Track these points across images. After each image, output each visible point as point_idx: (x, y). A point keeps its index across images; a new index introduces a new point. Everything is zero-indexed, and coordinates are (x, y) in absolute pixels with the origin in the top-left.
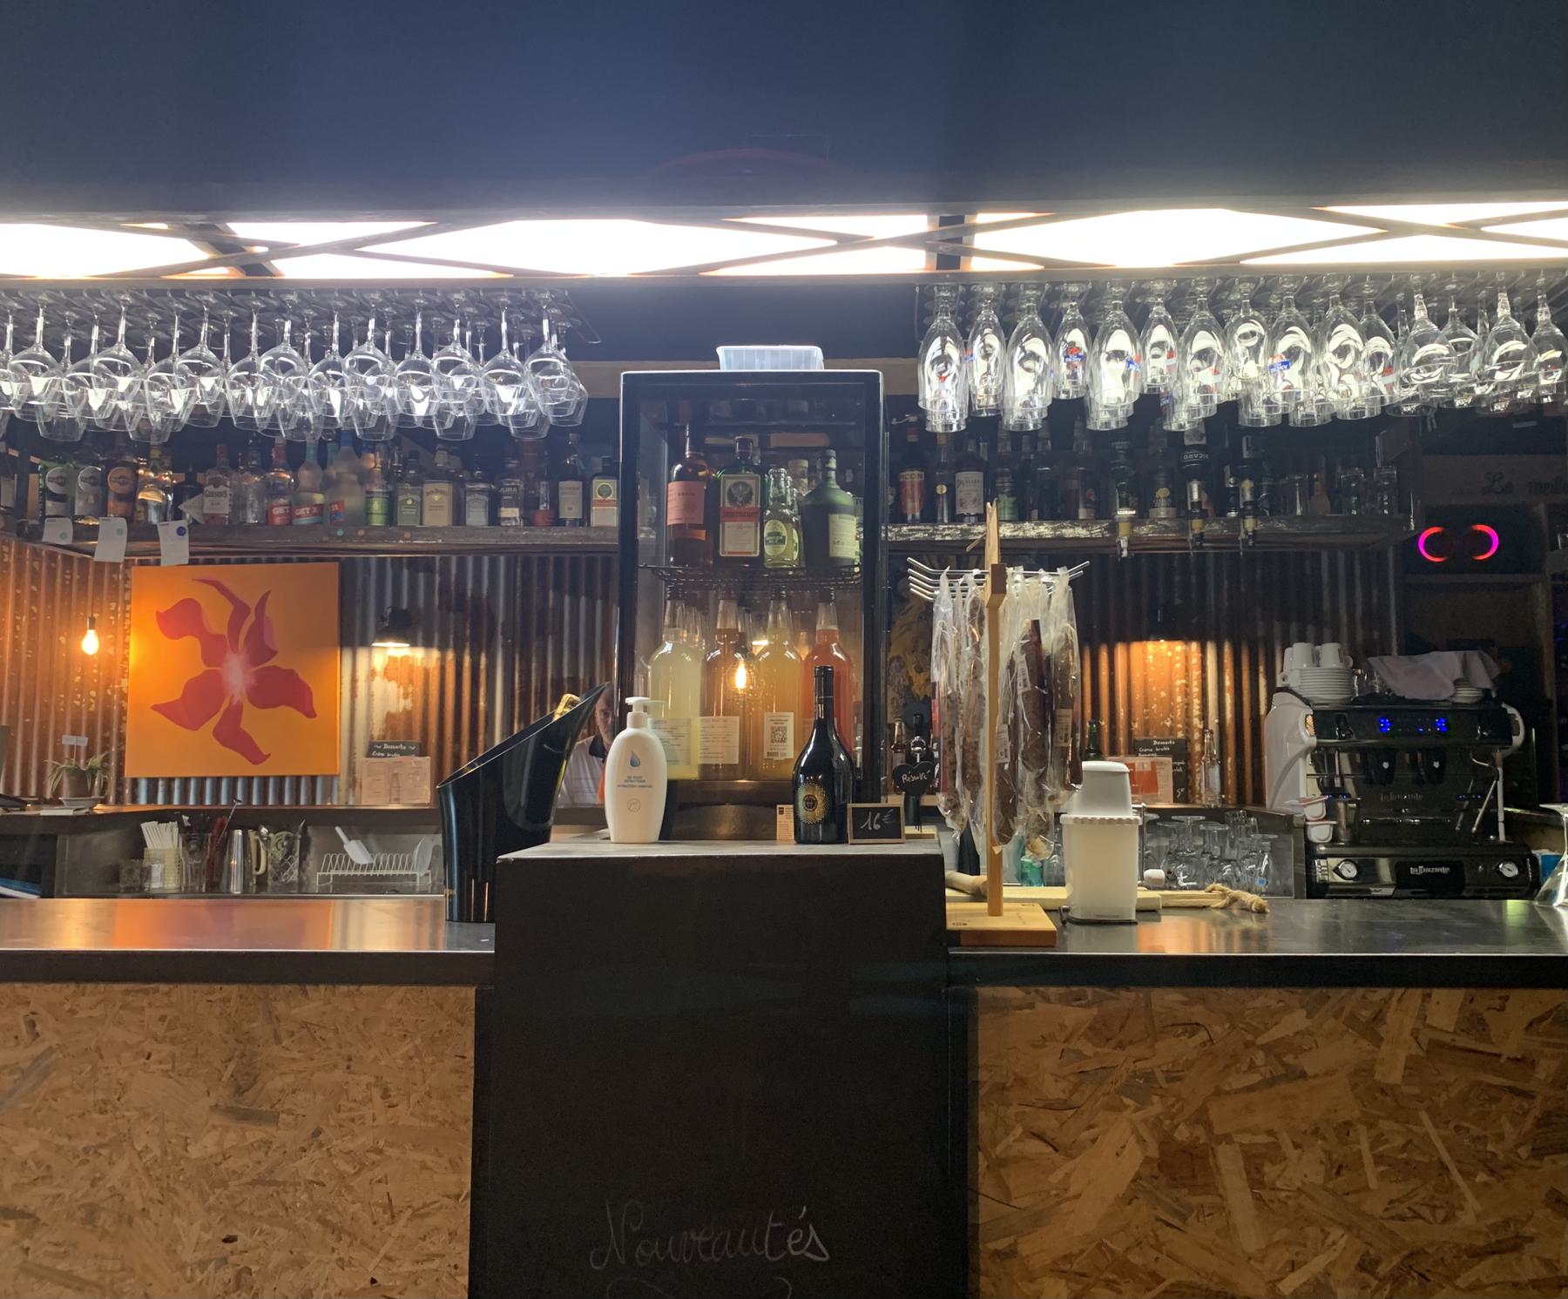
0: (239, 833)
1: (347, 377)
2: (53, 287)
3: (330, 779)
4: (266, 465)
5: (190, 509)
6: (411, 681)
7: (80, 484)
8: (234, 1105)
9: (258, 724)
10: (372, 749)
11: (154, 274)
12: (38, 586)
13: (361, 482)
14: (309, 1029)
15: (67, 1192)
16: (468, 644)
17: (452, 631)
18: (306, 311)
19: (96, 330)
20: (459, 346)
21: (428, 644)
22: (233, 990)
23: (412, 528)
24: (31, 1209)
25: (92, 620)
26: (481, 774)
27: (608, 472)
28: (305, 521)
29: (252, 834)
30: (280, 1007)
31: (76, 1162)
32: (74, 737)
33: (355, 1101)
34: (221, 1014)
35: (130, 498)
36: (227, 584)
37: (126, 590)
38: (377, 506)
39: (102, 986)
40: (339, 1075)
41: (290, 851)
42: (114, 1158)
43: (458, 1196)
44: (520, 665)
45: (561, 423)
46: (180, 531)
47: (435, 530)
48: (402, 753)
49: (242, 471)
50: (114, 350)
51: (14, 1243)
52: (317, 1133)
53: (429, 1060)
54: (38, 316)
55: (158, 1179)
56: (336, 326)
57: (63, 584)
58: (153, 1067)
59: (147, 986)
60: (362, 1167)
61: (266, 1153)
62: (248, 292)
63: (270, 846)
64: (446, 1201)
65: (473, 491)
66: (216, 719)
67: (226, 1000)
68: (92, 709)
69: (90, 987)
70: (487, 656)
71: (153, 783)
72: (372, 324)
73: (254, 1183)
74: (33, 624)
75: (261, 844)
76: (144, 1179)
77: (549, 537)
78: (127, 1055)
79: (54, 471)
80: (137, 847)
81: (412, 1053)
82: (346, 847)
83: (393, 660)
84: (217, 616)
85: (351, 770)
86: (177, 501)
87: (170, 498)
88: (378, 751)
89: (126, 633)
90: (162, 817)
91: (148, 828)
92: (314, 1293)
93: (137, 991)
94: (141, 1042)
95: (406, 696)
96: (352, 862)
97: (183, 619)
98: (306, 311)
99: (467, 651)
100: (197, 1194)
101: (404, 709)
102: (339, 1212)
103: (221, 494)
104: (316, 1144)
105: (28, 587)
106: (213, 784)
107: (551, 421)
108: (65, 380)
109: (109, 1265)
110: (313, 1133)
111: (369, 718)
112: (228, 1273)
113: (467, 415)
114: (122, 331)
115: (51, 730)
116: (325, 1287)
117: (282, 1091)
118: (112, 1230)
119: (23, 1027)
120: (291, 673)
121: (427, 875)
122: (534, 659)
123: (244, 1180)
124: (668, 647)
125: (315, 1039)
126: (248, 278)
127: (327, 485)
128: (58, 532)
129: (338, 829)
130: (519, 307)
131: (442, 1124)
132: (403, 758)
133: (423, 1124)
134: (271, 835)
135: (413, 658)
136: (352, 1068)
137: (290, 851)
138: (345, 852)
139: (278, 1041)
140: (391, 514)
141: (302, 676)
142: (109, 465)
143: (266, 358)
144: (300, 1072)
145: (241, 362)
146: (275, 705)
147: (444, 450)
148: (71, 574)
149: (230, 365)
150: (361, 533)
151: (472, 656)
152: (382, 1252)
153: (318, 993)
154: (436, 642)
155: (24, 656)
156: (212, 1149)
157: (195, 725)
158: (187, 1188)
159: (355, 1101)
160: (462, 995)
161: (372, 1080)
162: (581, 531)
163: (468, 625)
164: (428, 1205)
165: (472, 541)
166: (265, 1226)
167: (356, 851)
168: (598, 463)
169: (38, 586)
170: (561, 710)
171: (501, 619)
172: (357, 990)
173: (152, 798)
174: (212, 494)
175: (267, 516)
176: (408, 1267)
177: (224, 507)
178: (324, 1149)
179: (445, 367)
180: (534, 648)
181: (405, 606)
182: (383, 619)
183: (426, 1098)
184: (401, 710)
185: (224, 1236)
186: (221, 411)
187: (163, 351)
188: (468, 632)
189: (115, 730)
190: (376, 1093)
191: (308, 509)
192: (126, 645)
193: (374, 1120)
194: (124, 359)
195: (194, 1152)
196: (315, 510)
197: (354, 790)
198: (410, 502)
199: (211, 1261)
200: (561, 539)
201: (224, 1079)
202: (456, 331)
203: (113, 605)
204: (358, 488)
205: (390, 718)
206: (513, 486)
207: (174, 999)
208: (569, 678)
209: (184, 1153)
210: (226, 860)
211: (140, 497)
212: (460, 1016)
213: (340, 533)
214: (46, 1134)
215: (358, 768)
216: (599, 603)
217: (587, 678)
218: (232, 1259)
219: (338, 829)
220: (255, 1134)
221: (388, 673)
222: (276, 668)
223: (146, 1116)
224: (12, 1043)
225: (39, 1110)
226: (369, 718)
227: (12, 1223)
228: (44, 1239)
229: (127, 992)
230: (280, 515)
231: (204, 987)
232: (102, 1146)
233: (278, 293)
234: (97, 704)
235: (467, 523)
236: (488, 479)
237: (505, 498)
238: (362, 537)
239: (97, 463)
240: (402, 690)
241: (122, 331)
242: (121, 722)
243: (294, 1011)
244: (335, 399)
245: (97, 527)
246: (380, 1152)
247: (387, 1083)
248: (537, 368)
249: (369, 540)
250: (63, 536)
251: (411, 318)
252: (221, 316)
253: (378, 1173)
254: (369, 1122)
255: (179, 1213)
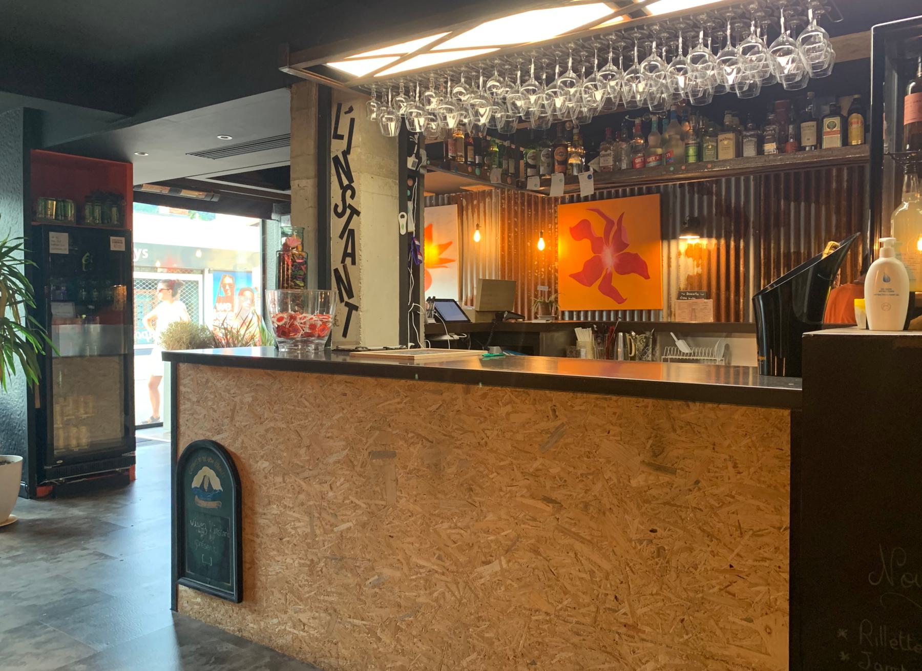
0: (621, 334)
1: (689, 68)
2: (538, 46)
3: (657, 312)
4: (631, 137)
5: (593, 166)
6: (701, 258)
7: (542, 158)
8: (653, 462)
9: (620, 282)
10: (681, 295)
11: (585, 28)
12: (517, 218)
13: (682, 139)
14: (691, 426)
15: (574, 494)
16: (733, 235)
17: (723, 227)
18: (663, 35)
19: (558, 67)
20: (754, 37)
21: (710, 236)
22: (650, 401)
23: (713, 162)
24: (559, 499)
25: (541, 233)
26: (779, 290)
27: (833, 114)
28: (652, 164)
29: (627, 335)
30: (675, 413)
31: (578, 480)
32: (542, 287)
33: (718, 467)
34: (644, 414)
35: (564, 163)
36: (603, 211)
37: (556, 217)
38: (692, 151)
39: (585, 395)
40: (708, 452)
41: (647, 345)
42: (595, 480)
43: (780, 528)
44: (764, 245)
45: (817, 76)
46: (589, 177)
47: (725, 161)
48: (697, 297)
49: (618, 142)
50: (567, 75)
51: (552, 515)
52: (697, 482)
53: (761, 449)
54: (531, 64)
55: (616, 495)
56: (681, 40)
57: (528, 216)
58: (611, 438)
59: (607, 396)
60: (723, 504)
61: (671, 489)
62: (632, 29)
63: (637, 341)
64: (772, 529)
65: (747, 136)
66: (600, 280)
67: (646, 407)
68: (543, 277)
69: (579, 395)
70: (744, 241)
71: (571, 313)
72: (701, 34)
73: (665, 504)
74: (516, 237)
75: (632, 340)
76: (610, 493)
77: (794, 158)
78: (598, 430)
79: (531, 152)
80: (573, 340)
81: (750, 444)
82: (676, 343)
83: (690, 246)
84: (598, 228)
85: (669, 307)
86: (587, 162)
87: (583, 160)
88: (683, 296)
89: (556, 239)
90: (584, 325)
91: (578, 331)
92: (699, 566)
93: (602, 399)
94: (604, 425)
95: (698, 266)
96: (680, 351)
97: (581, 231)
98: (663, 35)
99: (732, 239)
100: (636, 506)
101: (697, 273)
102: (711, 526)
103: (609, 155)
104: (697, 488)
105: (514, 219)
106: (599, 314)
107: (811, 75)
108: (544, 95)
109: (596, 533)
110: (695, 482)
111: (678, 278)
112: (653, 548)
113: (757, 80)
114: (570, 64)
115: (526, 288)
116: (704, 564)
117: (678, 458)
118: (596, 516)
119: (551, 413)
120: (636, 255)
121: (722, 360)
122: (772, 241)
123: (659, 501)
124: (906, 206)
125: (694, 432)
126: (633, 20)
127: (664, 143)
128: (533, 184)
129: (672, 334)
130: (791, 5)
131: (769, 486)
132: (697, 300)
133: (758, 485)
134: (637, 336)
135: (701, 244)
136: (716, 450)
137: (647, 345)
138: (676, 346)
139: (675, 431)
140: (699, 155)
141: (643, 258)
142: (555, 146)
143: (643, 64)
144: (687, 448)
145: (630, 69)
146: (628, 273)
147: (729, 114)
148: (531, 211)
149: (623, 73)
150: (683, 167)
151: (735, 242)
152: (735, 552)
153: (696, 407)
154: (714, 235)
155: (513, 253)
156: (642, 483)
157: (590, 284)
158: (631, 502)
159: (718, 467)
160: (781, 414)
161: (728, 457)
162: (816, 153)
163: (732, 224)
164: (763, 530)
165: (747, 165)
166: (672, 527)
167: (682, 345)
168: (826, 109)
169: (517, 218)
170: (827, 251)
171: (752, 219)
172: (718, 407)
173: (579, 318)
174: (604, 156)
175: (632, 164)
176: (750, 562)
177: (610, 162)
178: (701, 491)
179: (745, 52)
180: (772, 236)
181: (696, 215)
182: (685, 223)
183: (759, 471)
184: (695, 273)
185: (650, 529)
186: (618, 99)
187: (589, 72)
188: (733, 227)
189: (553, 287)
190: (730, 465)
191: (654, 158)
192: (556, 245)
193: (729, 479)
194: (572, 78)
195: (634, 483)
196: (658, 158)
197: (671, 317)
198: (710, 147)
199: (644, 540)
200: (803, 159)
201: (647, 448)
202: (752, 28)
203: (550, 225)
204: (680, 142)
205: (689, 278)
206: (771, 130)
207: (620, 404)
208: (794, 252)
209: (628, 483)
210: (615, 348)
211: (569, 162)
212: (779, 426)
213: (672, 169)
214: (563, 465)
215: (673, 306)
216: (813, 205)
217: (806, 252)
218: (655, 541)
219: (672, 334)
220: (664, 478)
221: (688, 253)
222: (629, 253)
223: (609, 462)
224: (545, 419)
225: (559, 453)
226: (678, 278)
227: (550, 505)
228: (565, 515)
229: (597, 399)
230: (639, 163)
231: (634, 399)
232: (590, 474)
233: (649, 26)
234: (545, 274)
235: (744, 155)
236: (757, 127)
237: (767, 137)
238: (685, 170)
239: (549, 147)
240: (695, 263)
241: (570, 64)
242: (556, 283)
243: (682, 416)
244: (681, 80)
245: (541, 187)
246: (733, 497)
247: (736, 460)
248: (806, 41)
249: (687, 171)
250: (536, 185)
251: (723, 27)
252: (618, 47)
253: (733, 508)
254: (726, 480)
255: (627, 513)
